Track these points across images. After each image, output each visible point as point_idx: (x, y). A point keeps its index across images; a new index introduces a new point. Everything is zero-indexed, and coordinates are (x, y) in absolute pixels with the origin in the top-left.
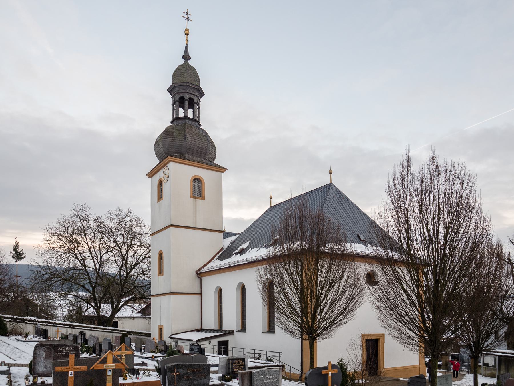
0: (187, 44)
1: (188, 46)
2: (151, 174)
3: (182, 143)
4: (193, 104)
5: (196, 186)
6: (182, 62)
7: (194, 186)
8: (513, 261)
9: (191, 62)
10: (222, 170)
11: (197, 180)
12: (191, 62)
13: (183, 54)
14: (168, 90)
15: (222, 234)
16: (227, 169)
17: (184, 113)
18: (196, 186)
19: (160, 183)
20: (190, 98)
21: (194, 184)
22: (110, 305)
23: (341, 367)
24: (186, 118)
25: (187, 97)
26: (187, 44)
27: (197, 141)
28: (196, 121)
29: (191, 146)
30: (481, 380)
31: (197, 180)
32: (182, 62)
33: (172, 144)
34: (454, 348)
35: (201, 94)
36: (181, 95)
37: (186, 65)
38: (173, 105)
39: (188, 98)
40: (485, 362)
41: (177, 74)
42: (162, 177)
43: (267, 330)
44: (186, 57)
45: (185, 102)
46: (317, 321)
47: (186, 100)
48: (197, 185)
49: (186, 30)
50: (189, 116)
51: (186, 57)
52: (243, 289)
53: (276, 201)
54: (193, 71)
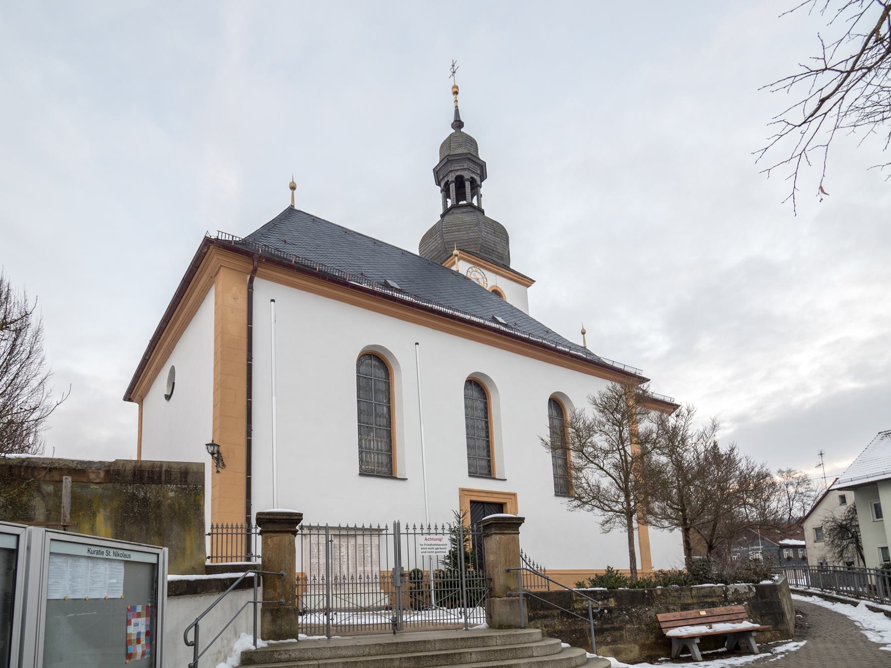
0: (457, 107)
1: (459, 108)
16: (534, 281)
26: (457, 107)
44: (458, 124)
51: (458, 124)
54: (472, 142)
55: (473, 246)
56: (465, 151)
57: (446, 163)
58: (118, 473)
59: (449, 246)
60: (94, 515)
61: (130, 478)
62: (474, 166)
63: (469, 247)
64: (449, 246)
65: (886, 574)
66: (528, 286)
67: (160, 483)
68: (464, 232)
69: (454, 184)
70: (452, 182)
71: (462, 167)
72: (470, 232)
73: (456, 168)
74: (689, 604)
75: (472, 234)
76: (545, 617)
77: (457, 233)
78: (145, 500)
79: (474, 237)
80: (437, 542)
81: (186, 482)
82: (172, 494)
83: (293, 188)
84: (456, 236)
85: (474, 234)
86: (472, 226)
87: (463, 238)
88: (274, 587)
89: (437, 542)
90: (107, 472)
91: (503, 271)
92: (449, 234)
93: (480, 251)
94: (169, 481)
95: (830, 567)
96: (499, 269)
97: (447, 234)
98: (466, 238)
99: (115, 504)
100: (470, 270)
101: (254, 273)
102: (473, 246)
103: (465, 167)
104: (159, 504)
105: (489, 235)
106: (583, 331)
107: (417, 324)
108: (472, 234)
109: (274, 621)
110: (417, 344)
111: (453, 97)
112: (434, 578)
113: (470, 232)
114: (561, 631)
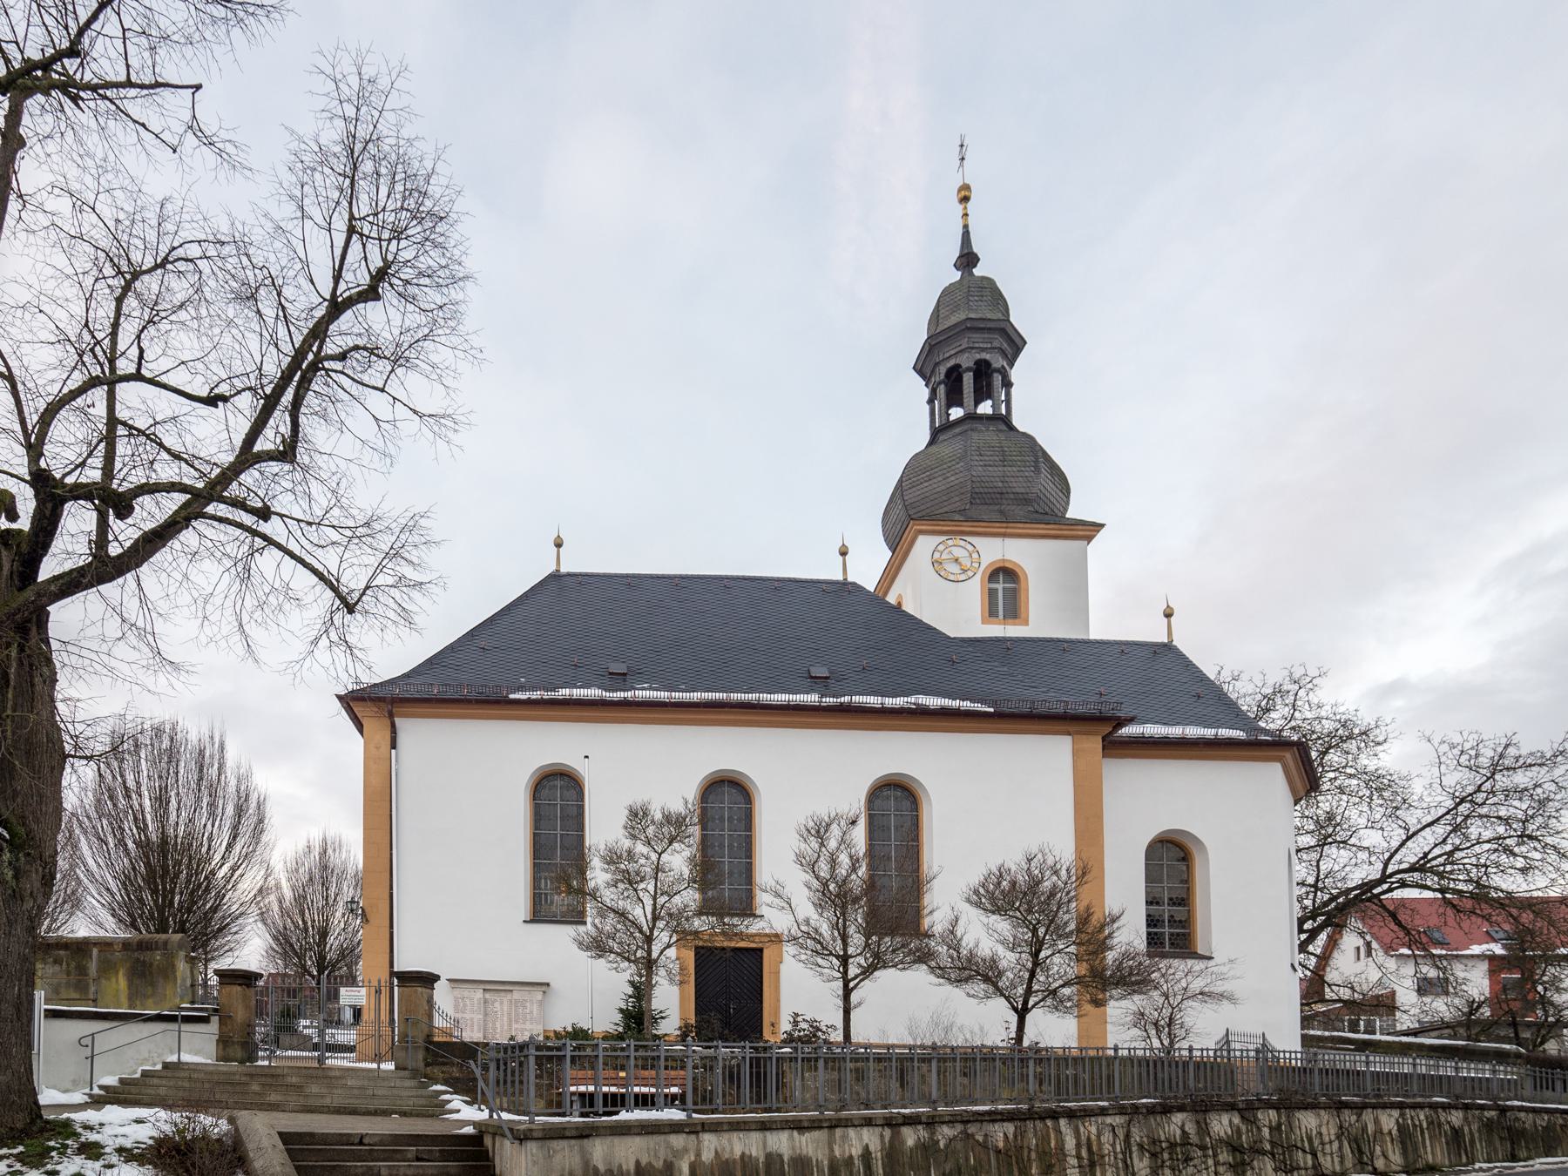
0: (966, 227)
1: (970, 229)
4: (988, 379)
6: (957, 275)
7: (992, 594)
8: (1566, 997)
10: (1089, 530)
14: (914, 368)
16: (1102, 526)
23: (1264, 1049)
25: (967, 361)
26: (966, 227)
28: (1003, 421)
31: (1005, 573)
34: (1403, 945)
35: (1014, 344)
38: (931, 401)
40: (406, 961)
44: (968, 259)
46: (45, 740)
48: (1004, 588)
51: (968, 259)
54: (990, 292)
55: (957, 499)
56: (963, 317)
57: (929, 351)
58: (129, 944)
59: (914, 511)
60: (117, 972)
61: (135, 947)
62: (983, 336)
63: (949, 502)
64: (914, 511)
65: (1550, 1076)
66: (1089, 539)
67: (152, 950)
68: (940, 479)
69: (942, 386)
70: (968, 369)
71: (959, 349)
72: (949, 475)
73: (947, 355)
74: (1173, 1107)
75: (952, 478)
76: (444, 1064)
77: (926, 484)
78: (144, 961)
79: (957, 482)
80: (357, 993)
81: (166, 949)
82: (158, 958)
83: (559, 545)
84: (926, 489)
85: (957, 476)
86: (953, 463)
87: (938, 490)
88: (226, 1024)
89: (357, 993)
90: (123, 944)
91: (1019, 528)
92: (914, 489)
93: (971, 503)
94: (157, 949)
95: (1234, 1050)
96: (1007, 528)
97: (910, 491)
98: (943, 488)
99: (128, 965)
100: (941, 548)
101: (391, 716)
102: (957, 499)
103: (963, 347)
104: (151, 965)
105: (990, 469)
106: (1168, 611)
107: (619, 722)
108: (952, 478)
109: (224, 1049)
110: (586, 757)
111: (959, 208)
112: (874, 1053)
113: (949, 475)
114: (457, 1079)
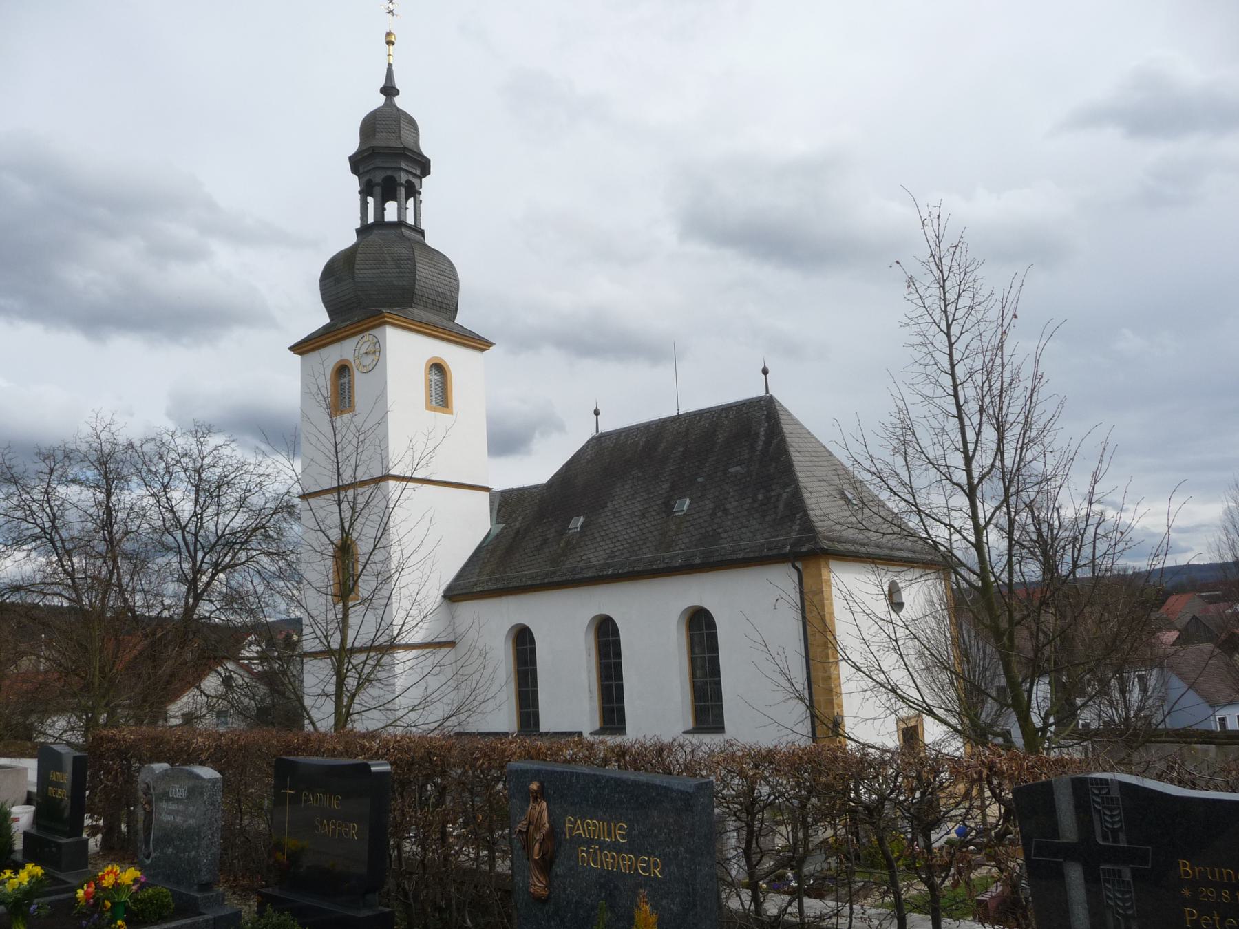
0: (390, 65)
2: (303, 348)
3: (405, 283)
5: (433, 382)
6: (380, 100)
9: (399, 101)
11: (438, 368)
12: (400, 102)
13: (382, 83)
15: (488, 493)
17: (384, 209)
18: (433, 382)
19: (343, 370)
20: (408, 182)
21: (431, 377)
22: (1078, 576)
24: (401, 224)
26: (390, 65)
27: (435, 279)
29: (424, 290)
30: (996, 927)
32: (380, 100)
33: (380, 284)
36: (389, 173)
37: (389, 103)
39: (403, 181)
41: (370, 126)
42: (351, 358)
43: (690, 725)
44: (389, 90)
45: (398, 188)
47: (401, 185)
49: (389, 34)
50: (408, 222)
51: (389, 90)
52: (523, 640)
53: (610, 424)
